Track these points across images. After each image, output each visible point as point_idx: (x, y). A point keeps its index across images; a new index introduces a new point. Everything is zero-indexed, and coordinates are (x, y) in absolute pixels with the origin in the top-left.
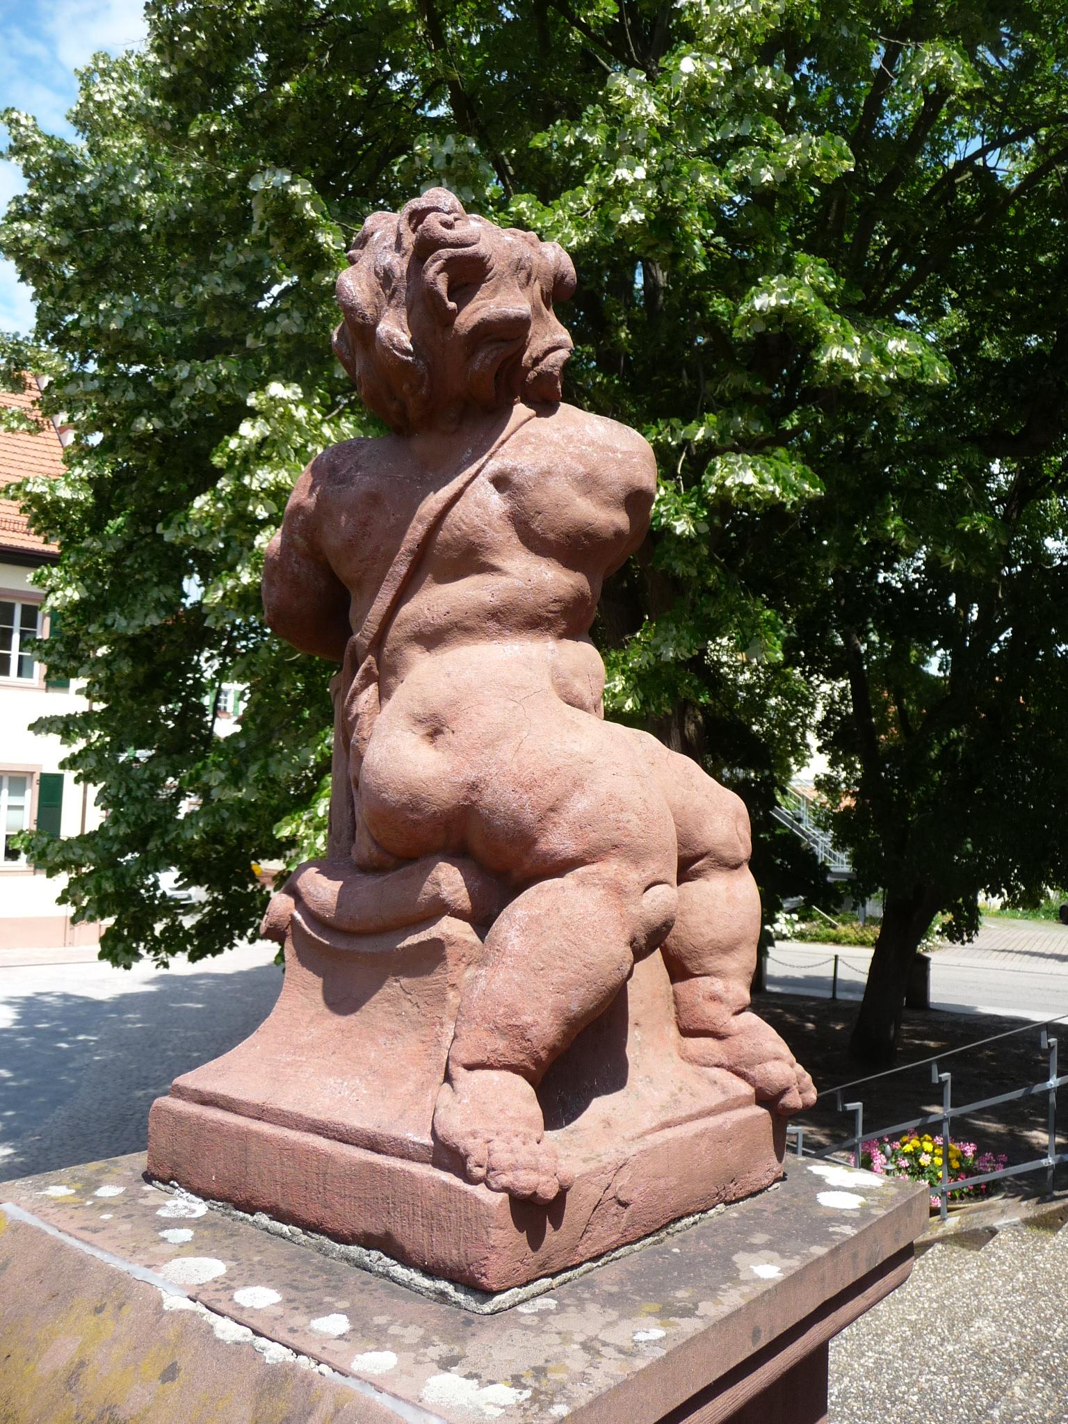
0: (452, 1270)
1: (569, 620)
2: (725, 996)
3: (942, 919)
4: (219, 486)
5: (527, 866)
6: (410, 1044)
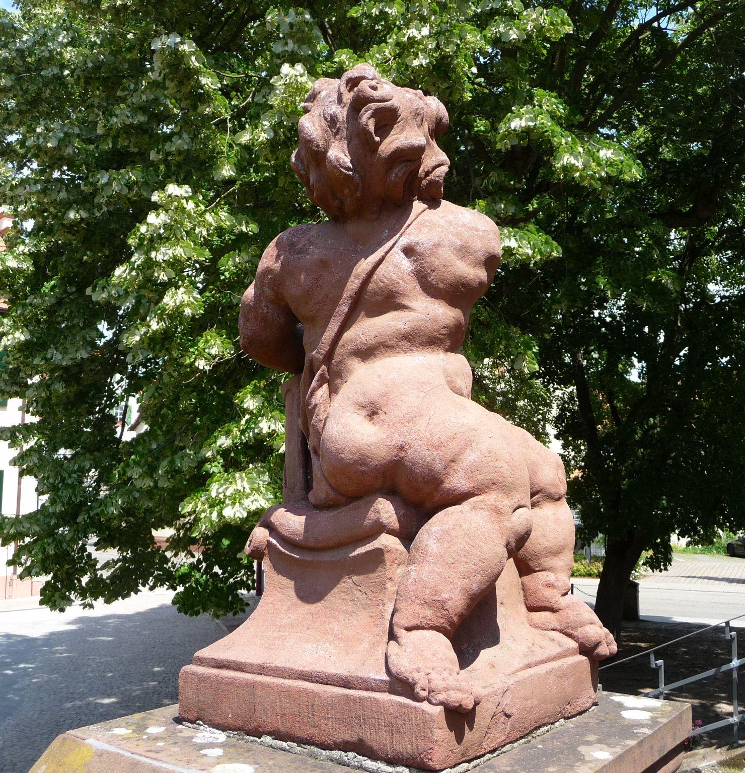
0: (407, 759)
1: (453, 340)
2: (556, 584)
3: (647, 554)
4: (133, 259)
5: (436, 499)
6: (362, 618)
